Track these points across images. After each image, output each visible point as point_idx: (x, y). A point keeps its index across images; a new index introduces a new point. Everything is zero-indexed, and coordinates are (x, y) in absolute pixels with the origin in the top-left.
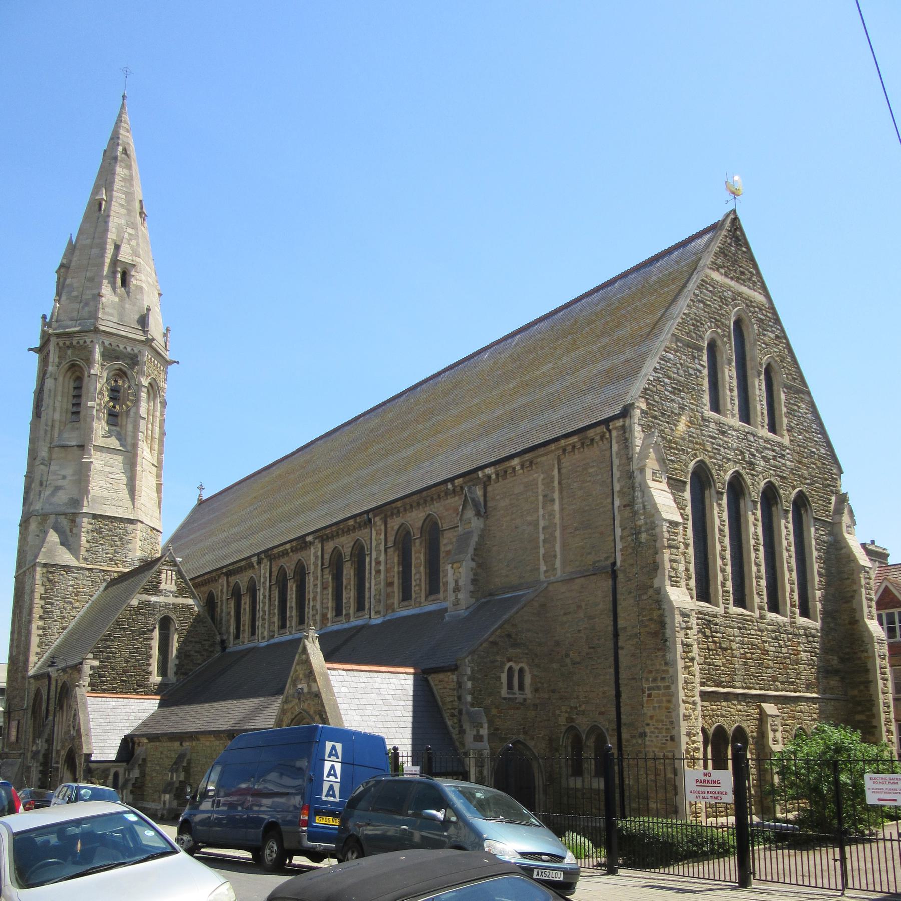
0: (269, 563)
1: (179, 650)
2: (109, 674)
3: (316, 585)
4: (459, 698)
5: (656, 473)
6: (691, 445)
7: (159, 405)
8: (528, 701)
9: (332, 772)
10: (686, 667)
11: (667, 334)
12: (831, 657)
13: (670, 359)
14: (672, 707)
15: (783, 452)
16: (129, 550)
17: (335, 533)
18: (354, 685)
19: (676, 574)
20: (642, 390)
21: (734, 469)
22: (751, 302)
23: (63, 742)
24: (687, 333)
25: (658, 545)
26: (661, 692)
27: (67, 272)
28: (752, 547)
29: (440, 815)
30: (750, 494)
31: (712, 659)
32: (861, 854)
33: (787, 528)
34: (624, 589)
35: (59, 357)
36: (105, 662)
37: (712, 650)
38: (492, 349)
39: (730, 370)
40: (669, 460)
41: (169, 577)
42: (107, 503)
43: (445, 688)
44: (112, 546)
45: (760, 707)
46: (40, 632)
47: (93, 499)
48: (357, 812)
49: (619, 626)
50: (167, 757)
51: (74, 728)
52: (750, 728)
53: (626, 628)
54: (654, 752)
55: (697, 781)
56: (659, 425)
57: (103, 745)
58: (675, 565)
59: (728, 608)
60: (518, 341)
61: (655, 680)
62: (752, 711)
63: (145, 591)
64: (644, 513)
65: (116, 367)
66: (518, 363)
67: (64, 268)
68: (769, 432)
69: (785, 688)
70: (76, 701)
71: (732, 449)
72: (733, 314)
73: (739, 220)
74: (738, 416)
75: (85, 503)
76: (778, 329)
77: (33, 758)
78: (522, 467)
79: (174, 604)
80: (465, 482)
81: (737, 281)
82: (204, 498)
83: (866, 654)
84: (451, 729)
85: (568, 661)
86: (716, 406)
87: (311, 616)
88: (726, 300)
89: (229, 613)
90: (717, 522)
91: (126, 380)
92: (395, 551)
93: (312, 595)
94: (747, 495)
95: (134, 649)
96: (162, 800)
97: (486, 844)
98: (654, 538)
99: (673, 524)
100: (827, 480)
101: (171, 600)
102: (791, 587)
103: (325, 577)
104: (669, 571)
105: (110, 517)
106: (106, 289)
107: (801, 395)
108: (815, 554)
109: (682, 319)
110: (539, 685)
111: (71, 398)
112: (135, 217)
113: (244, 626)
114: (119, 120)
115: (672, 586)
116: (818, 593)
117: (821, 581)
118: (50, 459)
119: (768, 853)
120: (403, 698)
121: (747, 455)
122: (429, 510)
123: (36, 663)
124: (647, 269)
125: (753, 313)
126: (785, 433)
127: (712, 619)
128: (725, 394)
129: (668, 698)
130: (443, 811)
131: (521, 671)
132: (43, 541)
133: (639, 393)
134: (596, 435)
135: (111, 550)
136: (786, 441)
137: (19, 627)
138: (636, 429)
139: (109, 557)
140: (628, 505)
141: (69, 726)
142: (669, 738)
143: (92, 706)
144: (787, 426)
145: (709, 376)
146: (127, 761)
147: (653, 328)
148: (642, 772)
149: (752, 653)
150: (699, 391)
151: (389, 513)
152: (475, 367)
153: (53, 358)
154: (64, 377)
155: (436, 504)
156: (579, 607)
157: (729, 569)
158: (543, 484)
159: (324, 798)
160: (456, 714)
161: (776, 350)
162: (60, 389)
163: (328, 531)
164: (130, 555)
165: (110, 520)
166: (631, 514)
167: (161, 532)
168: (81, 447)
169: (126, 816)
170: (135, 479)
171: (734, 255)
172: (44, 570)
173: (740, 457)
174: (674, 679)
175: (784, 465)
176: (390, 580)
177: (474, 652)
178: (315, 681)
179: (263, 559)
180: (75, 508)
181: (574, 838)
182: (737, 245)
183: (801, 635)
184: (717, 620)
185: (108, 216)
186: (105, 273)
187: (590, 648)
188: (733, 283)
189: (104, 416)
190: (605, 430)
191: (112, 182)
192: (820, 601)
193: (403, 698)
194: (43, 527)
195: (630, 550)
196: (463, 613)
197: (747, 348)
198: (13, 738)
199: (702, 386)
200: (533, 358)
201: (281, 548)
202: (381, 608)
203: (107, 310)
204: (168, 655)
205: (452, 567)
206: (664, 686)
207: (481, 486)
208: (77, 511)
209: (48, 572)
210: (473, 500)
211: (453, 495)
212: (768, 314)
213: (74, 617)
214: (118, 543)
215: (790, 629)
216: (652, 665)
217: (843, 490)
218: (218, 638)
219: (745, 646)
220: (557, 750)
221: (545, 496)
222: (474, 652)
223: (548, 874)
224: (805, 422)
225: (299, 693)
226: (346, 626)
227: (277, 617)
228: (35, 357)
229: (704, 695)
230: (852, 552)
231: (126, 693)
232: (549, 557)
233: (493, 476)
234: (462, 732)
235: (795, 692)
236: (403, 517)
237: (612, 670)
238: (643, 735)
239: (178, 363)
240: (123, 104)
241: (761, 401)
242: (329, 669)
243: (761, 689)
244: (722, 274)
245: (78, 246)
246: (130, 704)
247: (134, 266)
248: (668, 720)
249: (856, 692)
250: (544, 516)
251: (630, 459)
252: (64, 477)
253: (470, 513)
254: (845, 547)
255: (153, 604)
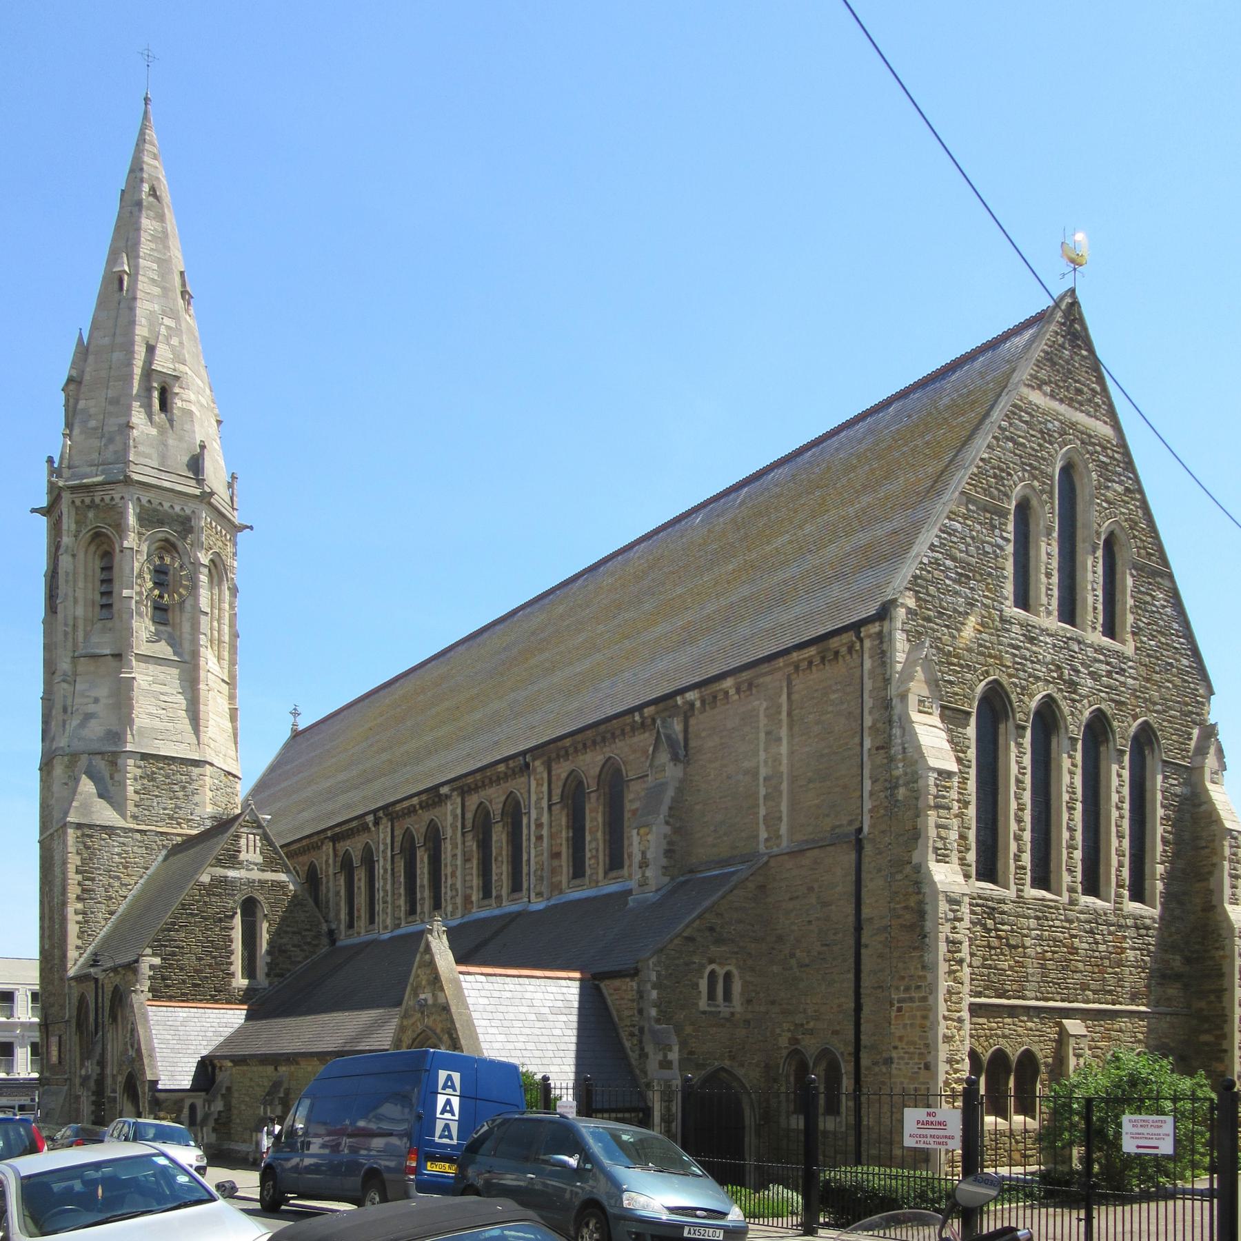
0: (389, 824)
1: (270, 943)
2: (176, 976)
3: (454, 856)
4: (641, 1011)
5: (924, 701)
6: (981, 659)
7: (227, 593)
8: (738, 1016)
9: (448, 1108)
10: (951, 972)
11: (953, 492)
12: (1171, 956)
13: (955, 530)
14: (928, 1024)
15: (1123, 666)
16: (196, 804)
17: (480, 784)
18: (496, 994)
19: (945, 845)
20: (909, 578)
21: (1045, 693)
22: (1090, 436)
23: (120, 1065)
24: (985, 490)
25: (921, 804)
26: (915, 1005)
27: (78, 390)
28: (1064, 804)
29: (573, 1161)
30: (1067, 728)
31: (995, 960)
32: (1144, 1214)
33: (1119, 776)
34: (873, 864)
35: (77, 522)
36: (169, 959)
37: (995, 948)
38: (708, 508)
39: (1049, 545)
40: (946, 681)
41: (251, 843)
42: (161, 737)
43: (623, 999)
44: (171, 799)
45: (1060, 1025)
46: (80, 918)
47: (142, 730)
48: (479, 1158)
49: (864, 916)
50: (259, 1085)
51: (132, 1046)
52: (1044, 1053)
53: (872, 918)
54: (902, 1083)
55: (918, 1122)
56: (934, 630)
57: (173, 1069)
58: (943, 833)
59: (1022, 891)
60: (745, 497)
61: (907, 989)
62: (1049, 1030)
63: (219, 863)
64: (904, 760)
65: (160, 535)
66: (742, 531)
67: (74, 383)
68: (1104, 635)
69: (1099, 999)
70: (133, 1012)
71: (1044, 663)
72: (1060, 456)
73: (1079, 306)
74: (1056, 613)
75: (129, 737)
76: (1130, 478)
77: (82, 1084)
78: (738, 691)
79: (260, 881)
80: (657, 713)
81: (1070, 405)
82: (301, 728)
83: (1221, 953)
84: (630, 1053)
85: (793, 962)
86: (1023, 599)
87: (449, 899)
88: (1051, 436)
89: (337, 893)
90: (1014, 769)
91: (176, 555)
92: (562, 809)
93: (449, 870)
94: (1063, 730)
95: (209, 942)
96: (254, 1139)
97: (625, 1196)
98: (916, 795)
99: (945, 774)
100: (1187, 704)
101: (256, 875)
102: (1119, 861)
103: (467, 844)
104: (934, 841)
105: (166, 757)
106: (138, 417)
107: (1159, 579)
108: (1160, 812)
109: (978, 467)
110: (753, 994)
111: (98, 583)
112: (175, 300)
113: (359, 911)
114: (142, 139)
115: (938, 861)
116: (1160, 869)
117: (1165, 851)
118: (75, 674)
119: (1028, 1212)
120: (564, 1011)
121: (1067, 671)
122: (609, 751)
123: (76, 960)
124: (938, 385)
125: (1092, 454)
126: (1129, 637)
127: (996, 906)
128: (1038, 580)
129: (924, 1013)
130: (577, 1156)
131: (728, 977)
132: (74, 792)
133: (905, 584)
134: (842, 645)
135: (170, 804)
136: (1129, 649)
137: (51, 910)
138: (898, 636)
139: (168, 814)
140: (882, 748)
141: (126, 1044)
142: (922, 1066)
143: (155, 1018)
144: (1132, 627)
145: (1015, 554)
146: (207, 1090)
147: (936, 482)
148: (886, 1108)
149: (1054, 952)
150: (998, 577)
151: (554, 755)
152: (681, 537)
153: (68, 523)
154: (86, 552)
155: (619, 744)
156: (811, 889)
157: (1027, 836)
158: (767, 716)
159: (437, 1140)
160: (637, 1032)
161: (1124, 510)
162: (81, 570)
163: (470, 780)
164: (198, 811)
165: (166, 762)
166: (885, 761)
167: (240, 779)
168: (118, 656)
169: (155, 1159)
170: (198, 703)
171: (1067, 362)
172: (79, 833)
173: (1055, 675)
174: (933, 988)
175: (1123, 684)
176: (555, 850)
177: (662, 950)
178: (442, 989)
179: (381, 818)
180: (115, 744)
181: (780, 1191)
182: (1073, 347)
183: (1128, 927)
184: (1005, 908)
185: (135, 299)
186: (135, 391)
187: (823, 945)
188: (1062, 408)
189: (147, 610)
190: (854, 639)
191: (137, 243)
192: (1162, 879)
193: (564, 1011)
194: (73, 771)
195: (882, 812)
196: (651, 897)
197: (1080, 507)
198: (54, 1058)
199: (1003, 569)
200: (765, 524)
201: (406, 804)
202: (544, 889)
203: (141, 448)
204: (256, 950)
205: (638, 834)
206: (914, 1002)
207: (681, 718)
208: (118, 750)
209: (83, 835)
210: (668, 737)
211: (622, 738)
212: (1116, 455)
213: (125, 897)
214: (181, 794)
215: (1112, 918)
216: (904, 969)
217: (1212, 719)
218: (324, 927)
219: (1045, 943)
220: (775, 1080)
221: (768, 733)
222: (662, 950)
223: (703, 1232)
224: (1162, 619)
225: (421, 1006)
226: (497, 912)
227: (403, 898)
228: (42, 522)
229: (975, 1010)
230: (1215, 810)
231: (201, 1001)
232: (772, 820)
233: (698, 704)
234: (643, 1055)
235: (1114, 1004)
236: (573, 762)
237: (851, 976)
238: (889, 1061)
239: (251, 528)
240: (146, 112)
241: (1094, 590)
242: (461, 973)
243: (1063, 1001)
244: (1045, 394)
245: (91, 349)
246: (207, 1015)
247: (177, 378)
248: (922, 1042)
249: (1203, 1004)
250: (766, 762)
251: (887, 681)
252: (96, 701)
253: (664, 757)
254: (1205, 803)
255: (232, 882)
